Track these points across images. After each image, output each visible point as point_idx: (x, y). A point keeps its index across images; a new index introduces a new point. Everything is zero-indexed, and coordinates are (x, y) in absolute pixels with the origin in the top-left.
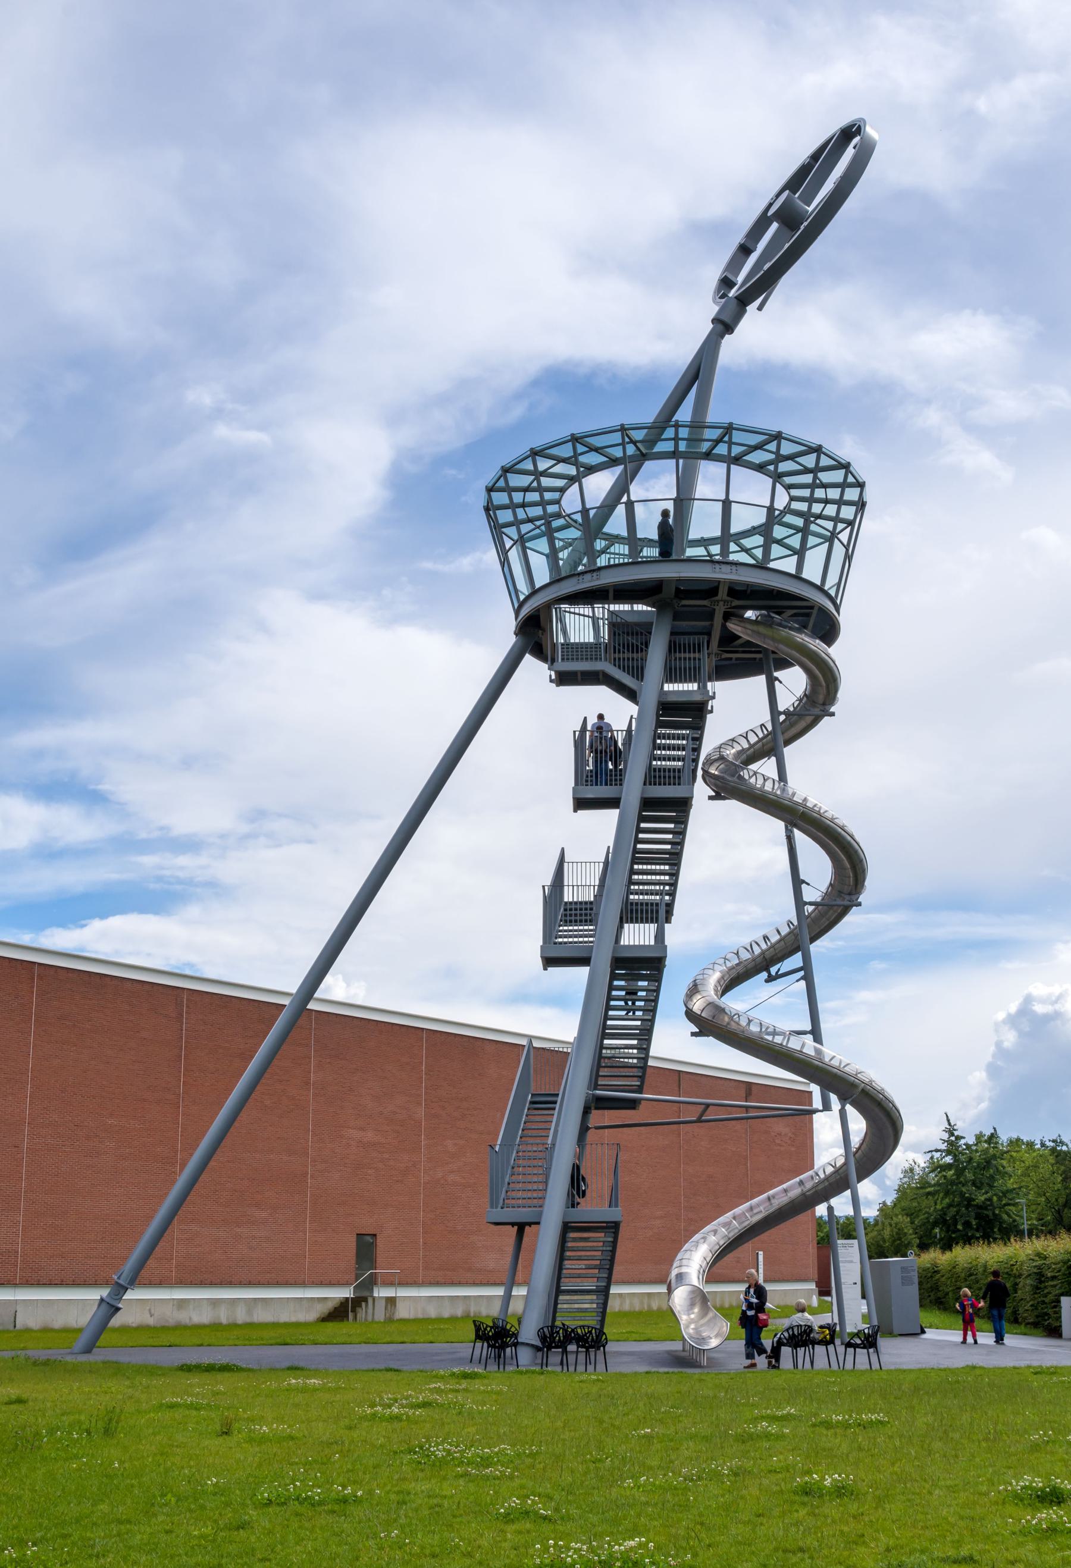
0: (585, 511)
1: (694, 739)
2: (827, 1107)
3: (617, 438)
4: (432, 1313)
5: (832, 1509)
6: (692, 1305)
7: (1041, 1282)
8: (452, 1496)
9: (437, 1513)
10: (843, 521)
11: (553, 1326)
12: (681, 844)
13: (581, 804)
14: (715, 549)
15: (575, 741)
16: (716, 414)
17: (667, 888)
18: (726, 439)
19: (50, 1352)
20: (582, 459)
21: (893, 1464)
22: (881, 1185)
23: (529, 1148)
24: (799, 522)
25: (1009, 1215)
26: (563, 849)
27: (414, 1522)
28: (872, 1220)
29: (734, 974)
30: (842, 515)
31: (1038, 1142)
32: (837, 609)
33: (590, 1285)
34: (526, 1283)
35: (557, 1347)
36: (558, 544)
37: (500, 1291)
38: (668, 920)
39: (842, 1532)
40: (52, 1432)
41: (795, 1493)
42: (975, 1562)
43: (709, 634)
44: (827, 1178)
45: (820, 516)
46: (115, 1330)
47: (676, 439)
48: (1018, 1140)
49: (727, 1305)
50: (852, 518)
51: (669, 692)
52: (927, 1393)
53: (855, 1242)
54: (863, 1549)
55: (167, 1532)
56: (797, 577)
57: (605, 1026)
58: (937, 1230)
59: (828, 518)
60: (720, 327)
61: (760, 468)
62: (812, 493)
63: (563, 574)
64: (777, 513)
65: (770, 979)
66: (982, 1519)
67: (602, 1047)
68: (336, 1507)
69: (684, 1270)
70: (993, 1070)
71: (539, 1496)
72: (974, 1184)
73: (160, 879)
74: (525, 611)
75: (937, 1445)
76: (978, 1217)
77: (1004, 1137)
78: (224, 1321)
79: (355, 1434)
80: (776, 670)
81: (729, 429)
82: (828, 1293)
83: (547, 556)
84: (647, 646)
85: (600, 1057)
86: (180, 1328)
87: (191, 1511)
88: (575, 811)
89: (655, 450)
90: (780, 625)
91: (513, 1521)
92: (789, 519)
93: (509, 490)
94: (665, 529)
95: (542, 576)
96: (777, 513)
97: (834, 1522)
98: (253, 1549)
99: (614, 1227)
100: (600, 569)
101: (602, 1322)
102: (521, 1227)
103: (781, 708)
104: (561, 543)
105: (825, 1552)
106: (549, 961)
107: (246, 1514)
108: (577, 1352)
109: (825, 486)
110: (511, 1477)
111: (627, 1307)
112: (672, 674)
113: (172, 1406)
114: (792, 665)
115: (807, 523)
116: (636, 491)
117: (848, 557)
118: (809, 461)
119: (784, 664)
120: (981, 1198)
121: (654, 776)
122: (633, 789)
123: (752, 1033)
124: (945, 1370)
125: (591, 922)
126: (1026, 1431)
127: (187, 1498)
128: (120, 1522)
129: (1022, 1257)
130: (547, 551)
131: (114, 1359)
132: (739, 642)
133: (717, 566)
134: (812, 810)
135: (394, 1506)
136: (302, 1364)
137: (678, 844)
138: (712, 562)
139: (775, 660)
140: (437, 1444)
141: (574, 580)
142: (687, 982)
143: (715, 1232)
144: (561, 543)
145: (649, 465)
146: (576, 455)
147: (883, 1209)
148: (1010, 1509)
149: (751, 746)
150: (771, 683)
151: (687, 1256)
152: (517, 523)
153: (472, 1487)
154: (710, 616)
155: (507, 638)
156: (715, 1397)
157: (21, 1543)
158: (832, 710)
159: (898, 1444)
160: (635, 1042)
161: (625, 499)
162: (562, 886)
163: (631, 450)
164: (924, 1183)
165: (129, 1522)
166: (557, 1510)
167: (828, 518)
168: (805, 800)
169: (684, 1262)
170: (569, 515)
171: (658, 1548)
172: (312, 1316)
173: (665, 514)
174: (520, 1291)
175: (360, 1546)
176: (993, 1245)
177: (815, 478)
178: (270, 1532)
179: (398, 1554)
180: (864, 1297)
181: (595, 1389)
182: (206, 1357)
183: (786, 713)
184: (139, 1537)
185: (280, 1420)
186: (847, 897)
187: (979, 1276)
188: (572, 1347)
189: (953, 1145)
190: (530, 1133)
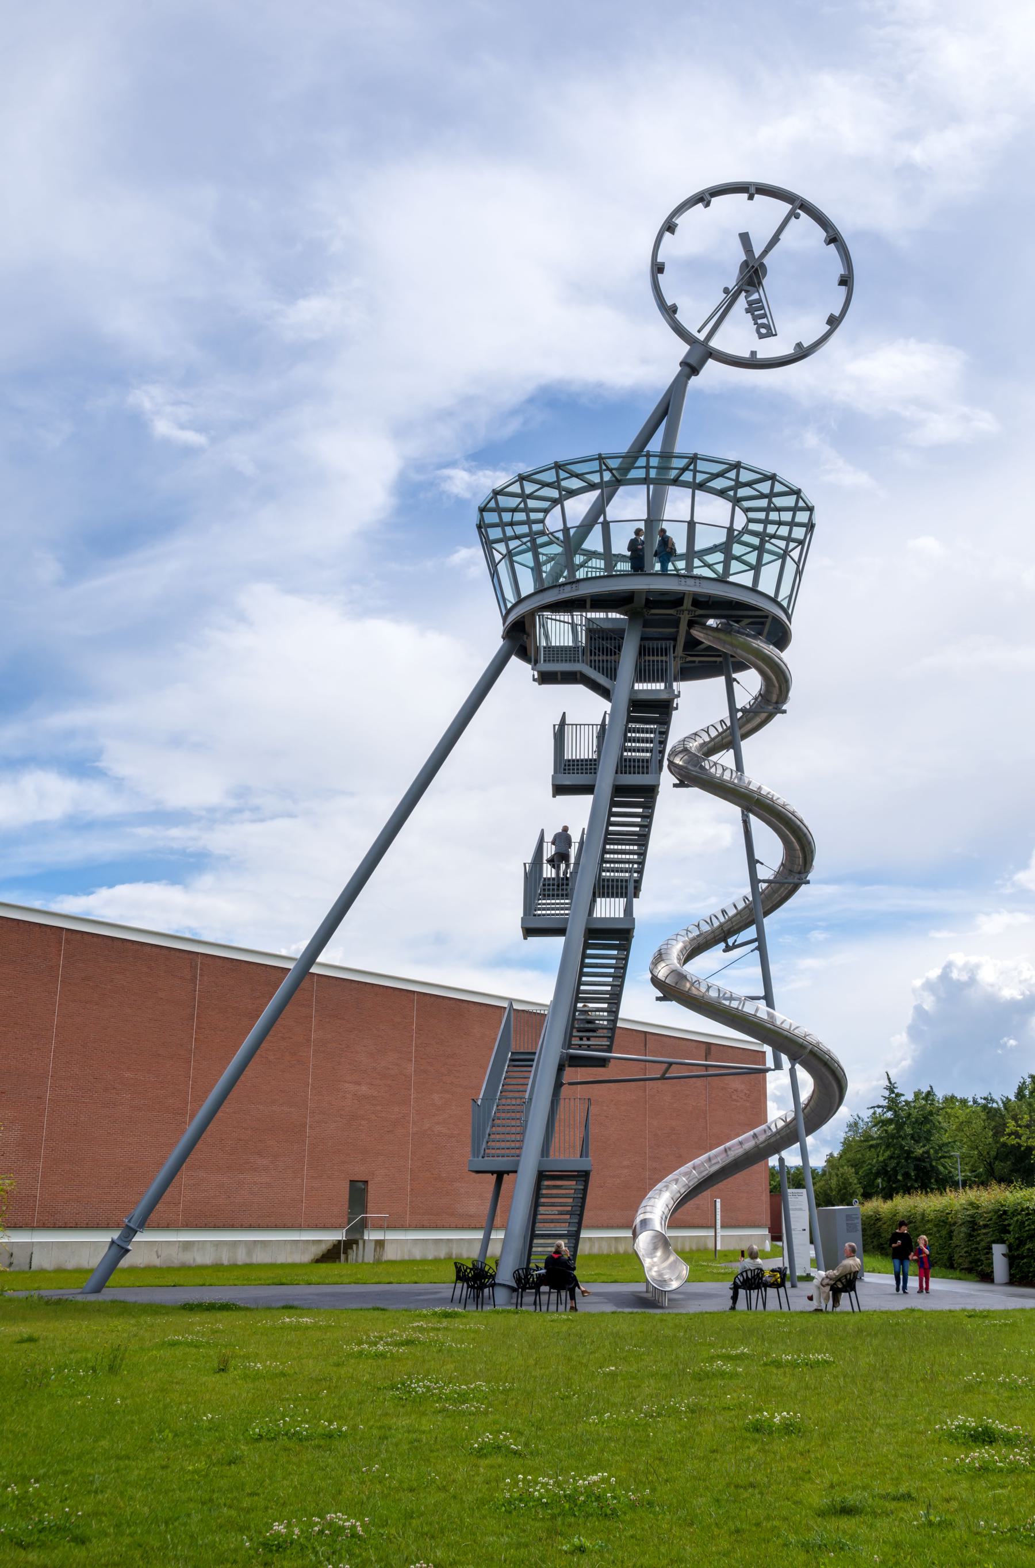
0: (566, 530)
1: (661, 733)
2: (778, 1066)
4: (417, 1255)
5: (780, 1446)
7: (974, 1230)
9: (416, 1448)
10: (794, 540)
12: (649, 826)
13: (559, 790)
15: (555, 734)
16: (679, 448)
17: (636, 866)
18: (692, 467)
20: (564, 483)
21: (838, 1403)
23: (509, 1101)
24: (756, 541)
25: (945, 1167)
26: (543, 831)
28: (820, 1171)
29: (695, 944)
30: (793, 536)
31: (970, 1099)
32: (789, 618)
34: (505, 1227)
35: (530, 1288)
36: (542, 558)
37: (479, 1235)
39: (789, 1467)
40: (60, 1369)
41: (747, 1430)
42: (913, 1499)
43: (675, 639)
44: (778, 1132)
45: (774, 536)
46: (124, 1270)
47: (647, 467)
48: (953, 1097)
49: (687, 1249)
50: (802, 537)
52: (869, 1334)
53: (804, 1191)
54: (808, 1485)
55: (163, 1467)
56: (754, 590)
57: (578, 992)
58: (879, 1180)
60: (687, 370)
61: (721, 493)
62: (767, 516)
63: (546, 586)
64: (736, 533)
65: (728, 949)
66: (919, 1457)
68: (322, 1443)
69: (648, 1216)
71: (511, 1431)
72: (913, 1138)
74: (511, 618)
75: (878, 1384)
76: (917, 1168)
77: (940, 1094)
78: (226, 1262)
79: (343, 1371)
81: (694, 459)
83: (532, 569)
84: (620, 650)
86: (184, 1268)
87: (186, 1446)
88: (554, 796)
90: (739, 632)
91: (485, 1456)
92: (746, 538)
93: (499, 510)
94: (633, 545)
95: (527, 586)
96: (736, 533)
98: (243, 1484)
99: (584, 1176)
102: (500, 1175)
103: (739, 706)
104: (545, 558)
105: (774, 1487)
106: (529, 932)
108: (550, 1293)
109: (779, 510)
110: (486, 1413)
111: (595, 1250)
112: (642, 675)
113: (174, 1344)
114: (749, 668)
115: (763, 542)
116: (613, 511)
117: (799, 573)
118: (765, 487)
119: (741, 667)
120: (919, 1151)
121: (625, 766)
122: (606, 779)
123: (710, 998)
124: (886, 1312)
125: (567, 896)
126: (960, 1372)
128: (119, 1458)
129: (957, 1207)
130: (532, 564)
131: (122, 1298)
132: (702, 647)
133: (683, 580)
134: (766, 797)
135: (375, 1441)
136: (296, 1303)
138: (678, 575)
140: (418, 1381)
141: (555, 591)
143: (677, 1181)
144: (545, 558)
149: (712, 740)
151: (651, 1203)
153: (449, 1422)
154: (676, 623)
155: (494, 640)
156: (675, 1336)
157: (24, 1480)
159: (842, 1384)
160: (605, 1006)
161: (601, 519)
163: (607, 476)
164: (867, 1137)
165: (128, 1458)
166: (526, 1445)
168: (760, 788)
169: (648, 1209)
170: (551, 534)
171: (619, 1482)
172: (306, 1257)
175: (343, 1480)
176: (930, 1195)
177: (770, 502)
180: (812, 1242)
181: (565, 1329)
182: (208, 1296)
183: (743, 710)
184: (136, 1472)
185: (274, 1357)
186: (797, 876)
187: (918, 1224)
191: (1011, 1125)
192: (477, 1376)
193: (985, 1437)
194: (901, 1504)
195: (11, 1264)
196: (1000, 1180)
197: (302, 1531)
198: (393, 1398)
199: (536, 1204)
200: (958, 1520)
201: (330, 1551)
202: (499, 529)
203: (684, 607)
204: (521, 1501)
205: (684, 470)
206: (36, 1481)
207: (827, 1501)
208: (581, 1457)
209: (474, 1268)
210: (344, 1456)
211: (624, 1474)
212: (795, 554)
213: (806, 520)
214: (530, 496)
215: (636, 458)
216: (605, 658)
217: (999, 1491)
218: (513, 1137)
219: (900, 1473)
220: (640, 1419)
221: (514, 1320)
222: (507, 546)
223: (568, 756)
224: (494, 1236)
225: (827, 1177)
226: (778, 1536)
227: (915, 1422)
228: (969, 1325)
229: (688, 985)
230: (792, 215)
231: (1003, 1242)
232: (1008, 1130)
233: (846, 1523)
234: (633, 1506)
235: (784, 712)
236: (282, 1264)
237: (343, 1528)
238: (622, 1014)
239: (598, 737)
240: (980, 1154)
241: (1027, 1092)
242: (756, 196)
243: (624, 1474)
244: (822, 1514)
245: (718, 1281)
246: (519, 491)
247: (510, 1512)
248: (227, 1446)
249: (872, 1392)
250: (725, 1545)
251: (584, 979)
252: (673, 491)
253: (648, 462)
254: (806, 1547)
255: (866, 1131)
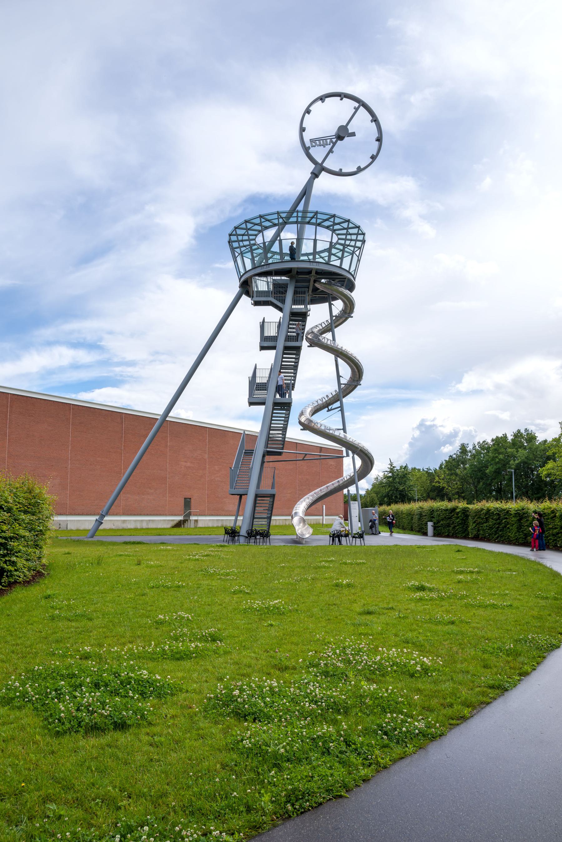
0: (264, 243)
1: (303, 325)
2: (348, 455)
3: (276, 216)
4: (210, 525)
5: (346, 591)
6: (300, 523)
7: (421, 517)
8: (215, 586)
9: (211, 591)
10: (357, 247)
11: (252, 530)
12: (298, 362)
13: (262, 348)
14: (311, 257)
15: (260, 326)
16: (311, 208)
17: (293, 378)
18: (315, 217)
19: (79, 537)
20: (263, 224)
21: (367, 577)
22: (367, 482)
23: (244, 468)
24: (341, 247)
25: (411, 494)
26: (256, 364)
27: (202, 594)
28: (363, 495)
29: (316, 408)
30: (356, 245)
31: (422, 469)
32: (355, 279)
33: (265, 516)
34: (243, 515)
35: (253, 537)
36: (255, 255)
37: (233, 518)
38: (293, 390)
39: (348, 599)
40: (79, 564)
41: (333, 586)
42: (394, 609)
43: (308, 288)
44: (347, 480)
45: (349, 245)
46: (101, 530)
47: (297, 217)
48: (415, 468)
49: (312, 523)
50: (360, 246)
51: (294, 308)
52: (380, 553)
53: (357, 502)
54: (355, 605)
55: (119, 596)
56: (340, 267)
57: (270, 427)
58: (386, 499)
59: (352, 246)
60: (314, 176)
61: (327, 227)
62: (346, 237)
63: (256, 266)
64: (333, 244)
65: (329, 410)
66: (397, 595)
67: (269, 434)
68: (176, 589)
69: (297, 511)
70: (411, 444)
71: (245, 586)
72: (399, 483)
73: (121, 376)
74: (242, 279)
75: (383, 571)
76: (400, 494)
77: (410, 467)
78: (139, 527)
79: (183, 565)
80: (332, 301)
81: (316, 213)
82: (347, 520)
83: (251, 259)
84: (286, 292)
85: (269, 437)
86: (123, 529)
87: (126, 590)
88: (260, 351)
89: (290, 221)
90: (334, 285)
91: (236, 594)
92: (338, 246)
93: (237, 235)
94: (291, 248)
95: (249, 266)
96: (333, 244)
97: (346, 595)
98: (148, 602)
99: (273, 496)
100: (269, 264)
101: (269, 528)
102: (241, 496)
103: (334, 314)
104: (256, 255)
105: (343, 605)
106: (251, 404)
107: (145, 591)
108: (260, 539)
109: (351, 234)
110: (236, 580)
111: (278, 524)
112: (295, 302)
113: (121, 555)
114: (338, 299)
115: (344, 248)
116: (283, 235)
117: (359, 260)
118: (345, 225)
119: (335, 299)
120: (401, 488)
121: (288, 338)
122: (281, 344)
123: (322, 429)
124: (387, 546)
125: (266, 390)
126: (413, 567)
127: (125, 586)
128: (102, 593)
129: (415, 508)
130: (251, 257)
131: (101, 540)
132: (319, 291)
133: (312, 263)
134: (344, 351)
135: (196, 589)
136: (165, 542)
137: (297, 363)
138: (310, 262)
139: (332, 297)
140: (211, 568)
141: (260, 268)
142: (299, 412)
143: (308, 498)
144: (256, 255)
145: (287, 226)
146: (261, 223)
147: (367, 491)
148: (406, 592)
149: (323, 328)
150: (330, 305)
151: (298, 506)
152: (240, 247)
153: (222, 583)
154: (309, 281)
155: (236, 288)
156: (307, 554)
157: (69, 599)
158: (352, 315)
159: (369, 570)
160: (281, 432)
161: (278, 239)
162: (255, 377)
163: (281, 221)
164: (381, 483)
165: (105, 593)
166: (251, 590)
167: (352, 246)
168: (342, 347)
169: (297, 508)
170: (258, 244)
171: (286, 603)
172: (169, 526)
173: (292, 243)
174: (241, 518)
175: (184, 601)
176: (405, 504)
177: (347, 231)
178: (153, 597)
179: (197, 604)
180: (359, 521)
181: (266, 551)
182: (132, 539)
183: (336, 316)
184: (109, 598)
185: (158, 560)
186: (356, 382)
187: (400, 515)
188: (258, 537)
189: (392, 470)
190: (244, 463)
191: (437, 478)
192: (233, 567)
193: (422, 588)
194: (389, 611)
195: (60, 528)
196: (432, 499)
197: (169, 618)
198: (202, 574)
199: (255, 506)
200: (410, 616)
201: (180, 624)
202: (237, 243)
203: (312, 275)
204: (249, 609)
205: (312, 218)
206: (73, 600)
207: (362, 610)
208: (271, 594)
209: (232, 530)
210: (184, 593)
211: (287, 600)
212: (357, 253)
213: (362, 239)
214: (250, 229)
215: (293, 213)
216: (280, 295)
217: (426, 607)
218: (246, 482)
219: (389, 600)
220: (294, 582)
221: (247, 548)
222: (241, 250)
223: (266, 334)
224: (239, 518)
225: (366, 497)
226: (344, 621)
227: (396, 584)
228: (418, 550)
229: (313, 424)
230: (357, 109)
231: (432, 521)
232: (435, 481)
233: (369, 617)
234: (290, 611)
235: (352, 317)
236: (160, 528)
237: (184, 617)
238: (288, 435)
239: (278, 327)
240: (425, 489)
241: (443, 466)
242: (344, 99)
243: (287, 600)
244: (360, 614)
245: (324, 535)
246: (245, 227)
247: (245, 613)
248: (142, 590)
249: (380, 573)
250: (324, 624)
251: (273, 422)
252: (307, 226)
253: (297, 214)
254: (354, 625)
255: (381, 481)
